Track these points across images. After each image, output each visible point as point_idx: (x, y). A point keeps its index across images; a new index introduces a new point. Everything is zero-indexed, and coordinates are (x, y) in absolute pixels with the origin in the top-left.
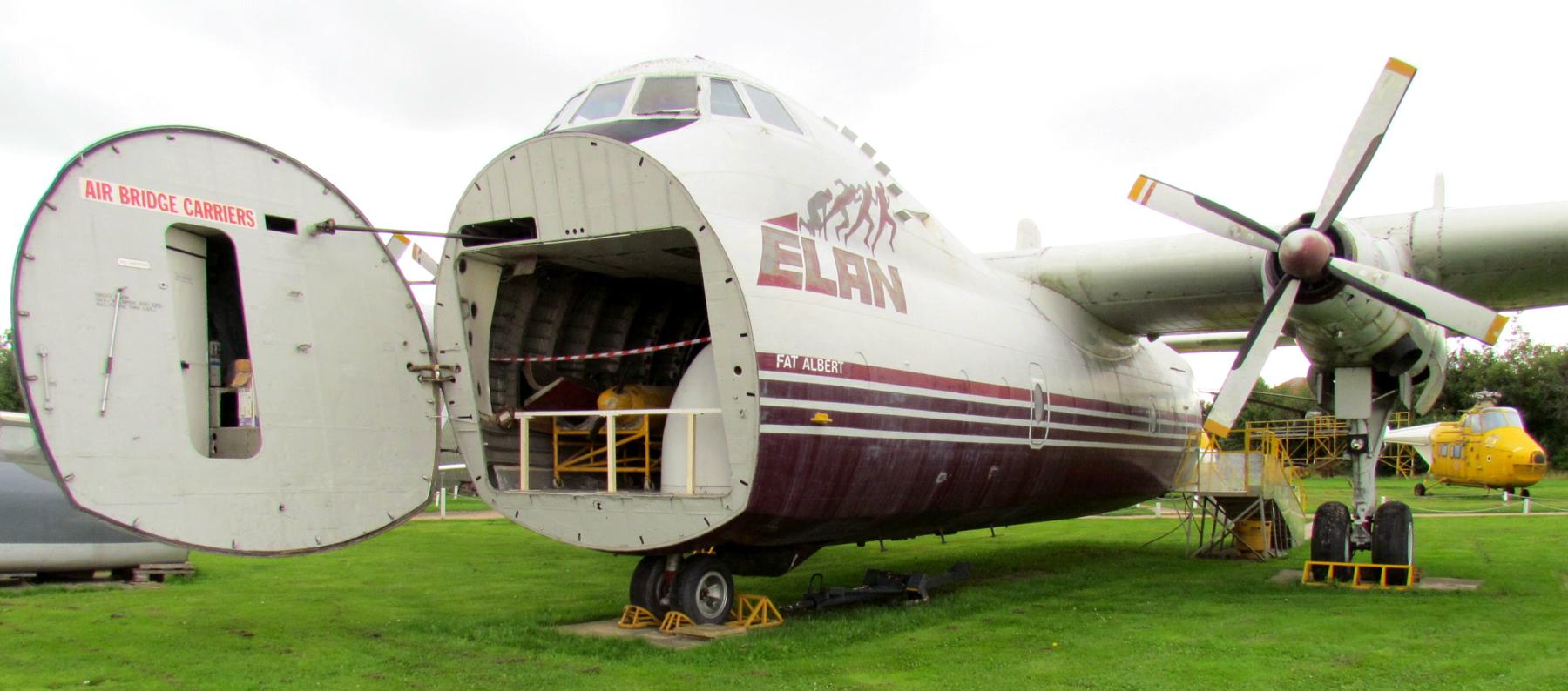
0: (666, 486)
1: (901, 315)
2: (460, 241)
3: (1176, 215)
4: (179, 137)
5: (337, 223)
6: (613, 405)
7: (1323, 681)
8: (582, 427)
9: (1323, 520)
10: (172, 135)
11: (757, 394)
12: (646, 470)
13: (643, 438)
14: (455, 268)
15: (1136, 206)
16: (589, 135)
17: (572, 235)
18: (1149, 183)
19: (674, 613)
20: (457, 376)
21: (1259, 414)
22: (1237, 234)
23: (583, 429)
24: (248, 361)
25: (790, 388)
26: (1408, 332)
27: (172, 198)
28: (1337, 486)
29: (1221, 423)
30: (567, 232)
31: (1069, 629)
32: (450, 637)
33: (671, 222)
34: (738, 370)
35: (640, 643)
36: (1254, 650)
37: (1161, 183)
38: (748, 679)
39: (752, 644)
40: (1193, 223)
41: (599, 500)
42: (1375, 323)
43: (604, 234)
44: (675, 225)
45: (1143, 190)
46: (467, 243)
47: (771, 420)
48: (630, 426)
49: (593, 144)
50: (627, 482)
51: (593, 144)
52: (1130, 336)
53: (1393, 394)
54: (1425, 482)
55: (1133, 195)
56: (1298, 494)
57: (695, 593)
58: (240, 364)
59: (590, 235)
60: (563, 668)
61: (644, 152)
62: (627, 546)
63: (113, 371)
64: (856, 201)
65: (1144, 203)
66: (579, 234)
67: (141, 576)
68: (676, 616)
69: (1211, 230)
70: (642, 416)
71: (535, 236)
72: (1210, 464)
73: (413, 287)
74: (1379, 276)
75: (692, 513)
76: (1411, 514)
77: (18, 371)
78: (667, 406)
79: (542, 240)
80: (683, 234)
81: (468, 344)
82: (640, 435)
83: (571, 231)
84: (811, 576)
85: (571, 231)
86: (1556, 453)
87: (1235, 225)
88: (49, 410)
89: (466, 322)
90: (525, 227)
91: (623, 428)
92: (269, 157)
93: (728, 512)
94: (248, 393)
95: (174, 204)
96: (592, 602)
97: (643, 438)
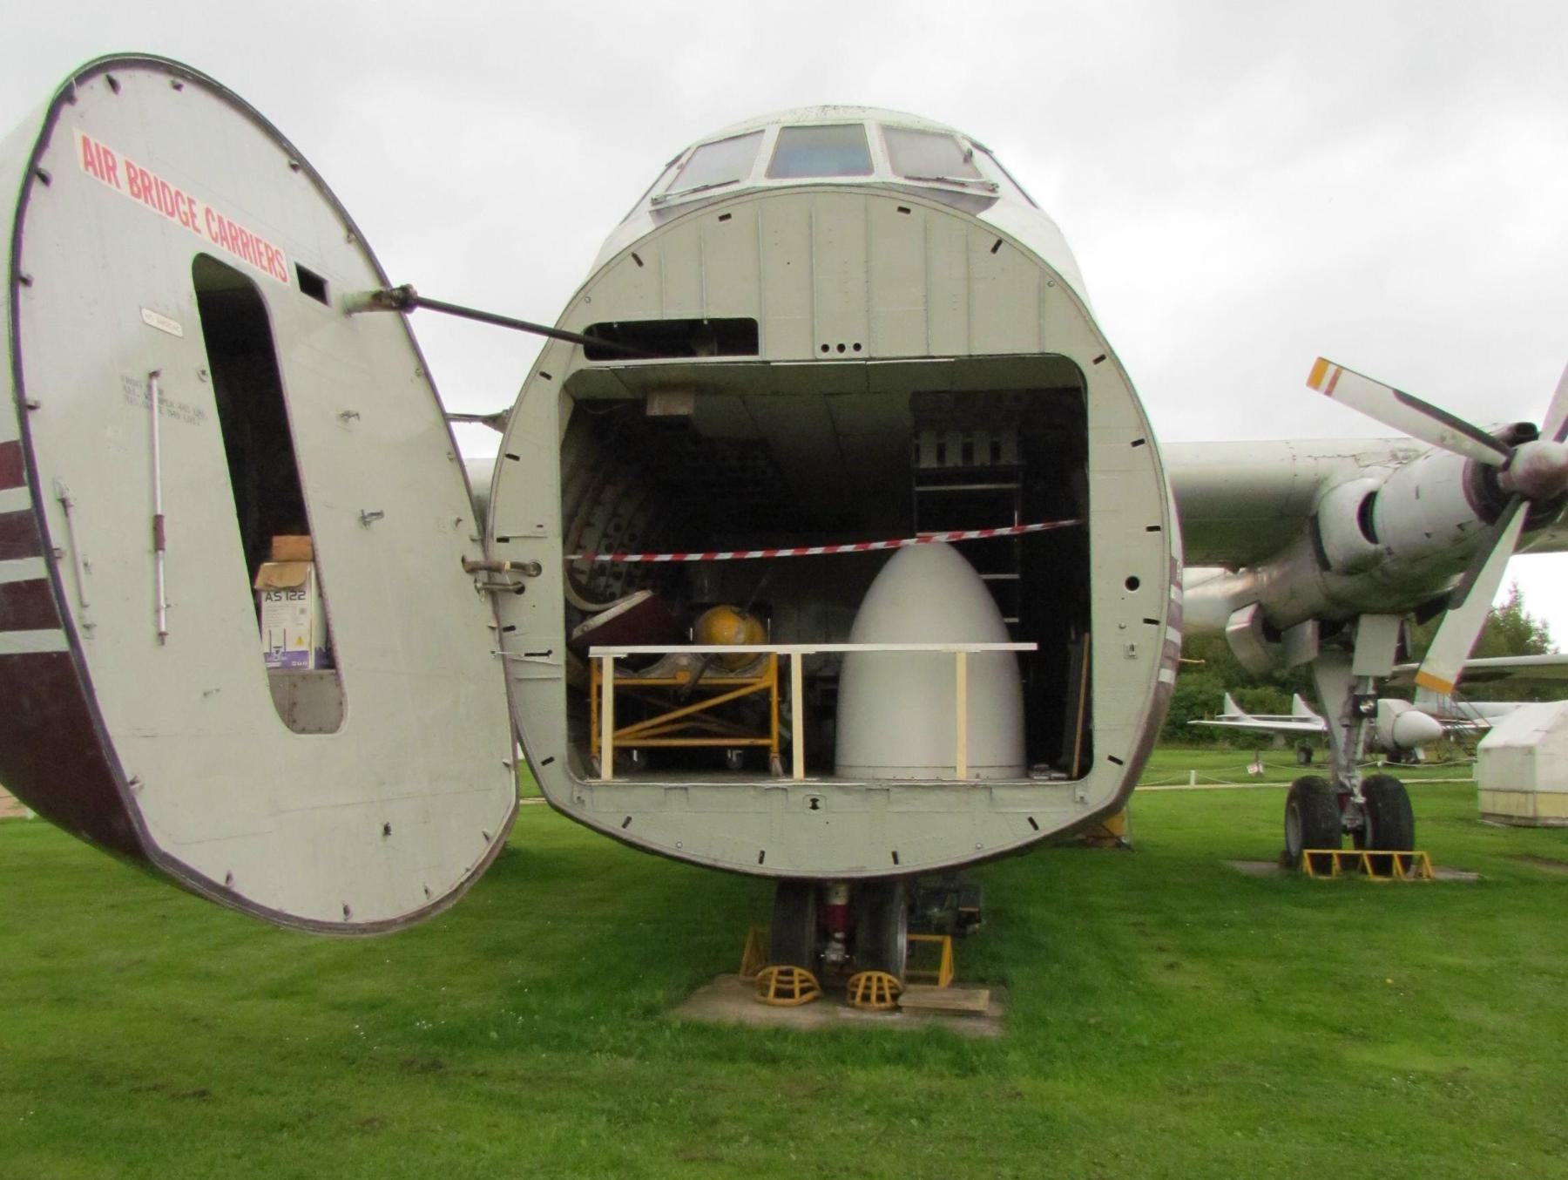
0: (845, 767)
2: (581, 347)
3: (1372, 412)
4: (189, 90)
5: (422, 293)
6: (742, 637)
8: (649, 672)
10: (179, 81)
11: (1163, 621)
12: (773, 742)
13: (768, 691)
15: (1318, 397)
16: (902, 196)
17: (833, 353)
18: (1331, 370)
19: (863, 976)
20: (530, 583)
22: (1449, 441)
23: (653, 675)
24: (306, 538)
27: (191, 202)
29: (1441, 677)
30: (825, 348)
33: (928, 351)
34: (1133, 583)
37: (1348, 370)
38: (518, 1030)
40: (1392, 423)
41: (816, 793)
43: (907, 355)
44: (1050, 349)
45: (1326, 377)
46: (592, 353)
48: (745, 671)
49: (901, 209)
50: (813, 768)
51: (901, 209)
55: (1314, 381)
58: (284, 544)
59: (874, 355)
61: (1004, 233)
62: (862, 869)
63: (168, 544)
65: (1329, 393)
66: (849, 353)
68: (869, 979)
69: (1418, 434)
70: (768, 654)
71: (753, 348)
73: (454, 425)
75: (1010, 810)
78: (845, 637)
79: (768, 359)
80: (1064, 364)
82: (761, 684)
83: (833, 347)
85: (833, 347)
87: (1448, 430)
88: (87, 627)
90: (741, 334)
91: (732, 675)
92: (284, 160)
93: (1079, 807)
94: (299, 604)
97: (768, 691)
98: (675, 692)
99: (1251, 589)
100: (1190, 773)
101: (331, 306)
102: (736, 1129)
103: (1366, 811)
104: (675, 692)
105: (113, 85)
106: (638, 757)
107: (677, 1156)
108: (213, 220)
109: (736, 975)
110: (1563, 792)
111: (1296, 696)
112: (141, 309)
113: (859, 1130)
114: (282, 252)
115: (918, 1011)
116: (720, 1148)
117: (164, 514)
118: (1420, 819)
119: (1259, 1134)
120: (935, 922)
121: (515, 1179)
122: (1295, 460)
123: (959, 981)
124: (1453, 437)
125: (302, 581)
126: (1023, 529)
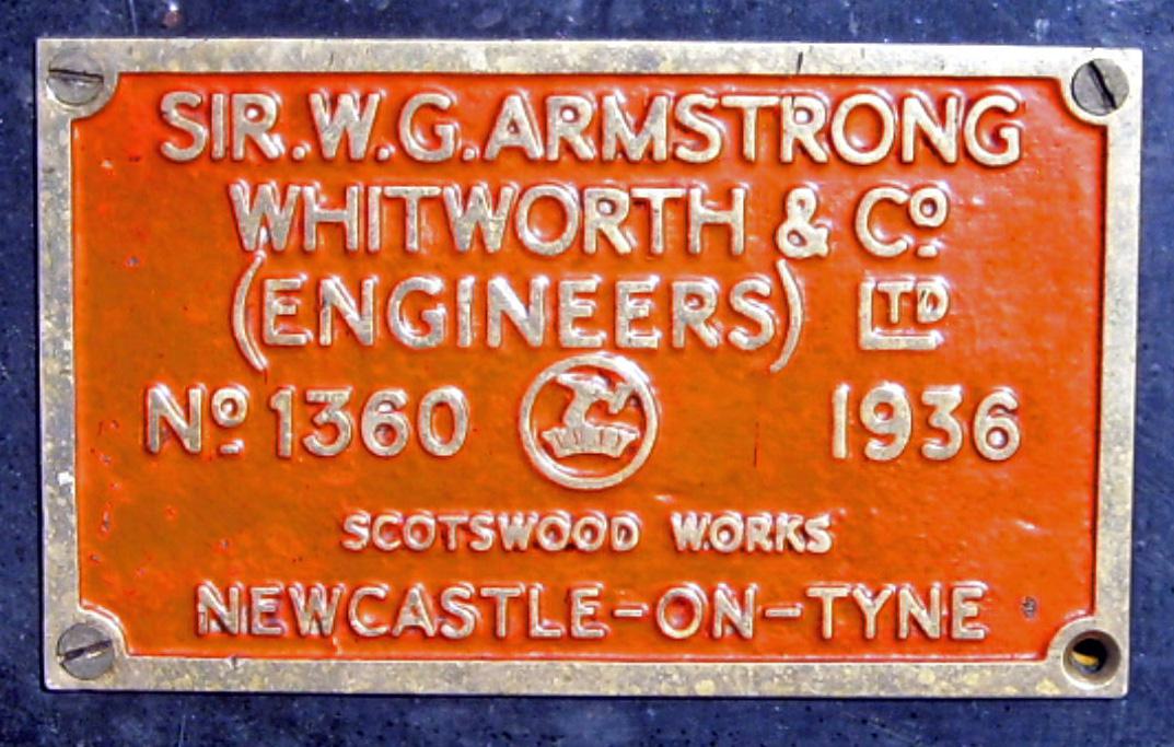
1: (684, 296)
7: (292, 723)
9: (1002, 705)
14: (1072, 642)
21: (1045, 31)
25: (136, 31)
26: (432, 328)
28: (755, 68)
31: (475, 430)
32: (691, 320)
35: (748, 681)
36: (571, 546)
39: (1011, 6)
42: (906, 191)
47: (1146, 325)
52: (167, 16)
53: (709, 499)
54: (142, 163)
56: (217, 13)
57: (639, 471)
60: (469, 674)
64: (577, 361)
67: (521, 53)
72: (18, 34)
73: (803, 72)
74: (1124, 385)
76: (789, 512)
77: (894, 182)
81: (508, 311)
84: (208, 426)
86: (1007, 26)
89: (1103, 40)
95: (931, 409)
96: (1073, 615)
98: (679, 30)
99: (433, 274)
100: (829, 96)
101: (519, 137)
102: (853, 734)
103: (923, 276)
104: (679, 30)
105: (1007, 708)
106: (326, 241)
107: (1125, 314)
108: (578, 379)
109: (631, 317)
110: (143, 78)
111: (350, 389)
112: (221, 455)
113: (112, 485)
114: (1041, 664)
115: (598, 628)
116: (621, 286)
117: (893, 432)
118: (158, 686)
119: (205, 99)
120: (884, 34)
121: (1112, 3)
122: (301, 559)
123: (621, 226)
124: (763, 50)
125: (260, 215)
126: (291, 203)
